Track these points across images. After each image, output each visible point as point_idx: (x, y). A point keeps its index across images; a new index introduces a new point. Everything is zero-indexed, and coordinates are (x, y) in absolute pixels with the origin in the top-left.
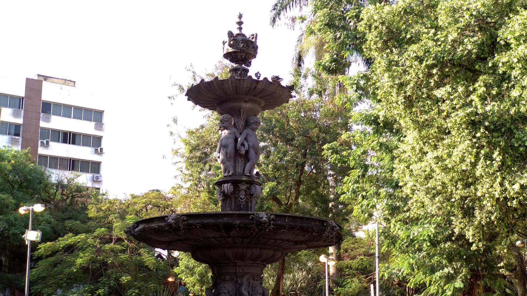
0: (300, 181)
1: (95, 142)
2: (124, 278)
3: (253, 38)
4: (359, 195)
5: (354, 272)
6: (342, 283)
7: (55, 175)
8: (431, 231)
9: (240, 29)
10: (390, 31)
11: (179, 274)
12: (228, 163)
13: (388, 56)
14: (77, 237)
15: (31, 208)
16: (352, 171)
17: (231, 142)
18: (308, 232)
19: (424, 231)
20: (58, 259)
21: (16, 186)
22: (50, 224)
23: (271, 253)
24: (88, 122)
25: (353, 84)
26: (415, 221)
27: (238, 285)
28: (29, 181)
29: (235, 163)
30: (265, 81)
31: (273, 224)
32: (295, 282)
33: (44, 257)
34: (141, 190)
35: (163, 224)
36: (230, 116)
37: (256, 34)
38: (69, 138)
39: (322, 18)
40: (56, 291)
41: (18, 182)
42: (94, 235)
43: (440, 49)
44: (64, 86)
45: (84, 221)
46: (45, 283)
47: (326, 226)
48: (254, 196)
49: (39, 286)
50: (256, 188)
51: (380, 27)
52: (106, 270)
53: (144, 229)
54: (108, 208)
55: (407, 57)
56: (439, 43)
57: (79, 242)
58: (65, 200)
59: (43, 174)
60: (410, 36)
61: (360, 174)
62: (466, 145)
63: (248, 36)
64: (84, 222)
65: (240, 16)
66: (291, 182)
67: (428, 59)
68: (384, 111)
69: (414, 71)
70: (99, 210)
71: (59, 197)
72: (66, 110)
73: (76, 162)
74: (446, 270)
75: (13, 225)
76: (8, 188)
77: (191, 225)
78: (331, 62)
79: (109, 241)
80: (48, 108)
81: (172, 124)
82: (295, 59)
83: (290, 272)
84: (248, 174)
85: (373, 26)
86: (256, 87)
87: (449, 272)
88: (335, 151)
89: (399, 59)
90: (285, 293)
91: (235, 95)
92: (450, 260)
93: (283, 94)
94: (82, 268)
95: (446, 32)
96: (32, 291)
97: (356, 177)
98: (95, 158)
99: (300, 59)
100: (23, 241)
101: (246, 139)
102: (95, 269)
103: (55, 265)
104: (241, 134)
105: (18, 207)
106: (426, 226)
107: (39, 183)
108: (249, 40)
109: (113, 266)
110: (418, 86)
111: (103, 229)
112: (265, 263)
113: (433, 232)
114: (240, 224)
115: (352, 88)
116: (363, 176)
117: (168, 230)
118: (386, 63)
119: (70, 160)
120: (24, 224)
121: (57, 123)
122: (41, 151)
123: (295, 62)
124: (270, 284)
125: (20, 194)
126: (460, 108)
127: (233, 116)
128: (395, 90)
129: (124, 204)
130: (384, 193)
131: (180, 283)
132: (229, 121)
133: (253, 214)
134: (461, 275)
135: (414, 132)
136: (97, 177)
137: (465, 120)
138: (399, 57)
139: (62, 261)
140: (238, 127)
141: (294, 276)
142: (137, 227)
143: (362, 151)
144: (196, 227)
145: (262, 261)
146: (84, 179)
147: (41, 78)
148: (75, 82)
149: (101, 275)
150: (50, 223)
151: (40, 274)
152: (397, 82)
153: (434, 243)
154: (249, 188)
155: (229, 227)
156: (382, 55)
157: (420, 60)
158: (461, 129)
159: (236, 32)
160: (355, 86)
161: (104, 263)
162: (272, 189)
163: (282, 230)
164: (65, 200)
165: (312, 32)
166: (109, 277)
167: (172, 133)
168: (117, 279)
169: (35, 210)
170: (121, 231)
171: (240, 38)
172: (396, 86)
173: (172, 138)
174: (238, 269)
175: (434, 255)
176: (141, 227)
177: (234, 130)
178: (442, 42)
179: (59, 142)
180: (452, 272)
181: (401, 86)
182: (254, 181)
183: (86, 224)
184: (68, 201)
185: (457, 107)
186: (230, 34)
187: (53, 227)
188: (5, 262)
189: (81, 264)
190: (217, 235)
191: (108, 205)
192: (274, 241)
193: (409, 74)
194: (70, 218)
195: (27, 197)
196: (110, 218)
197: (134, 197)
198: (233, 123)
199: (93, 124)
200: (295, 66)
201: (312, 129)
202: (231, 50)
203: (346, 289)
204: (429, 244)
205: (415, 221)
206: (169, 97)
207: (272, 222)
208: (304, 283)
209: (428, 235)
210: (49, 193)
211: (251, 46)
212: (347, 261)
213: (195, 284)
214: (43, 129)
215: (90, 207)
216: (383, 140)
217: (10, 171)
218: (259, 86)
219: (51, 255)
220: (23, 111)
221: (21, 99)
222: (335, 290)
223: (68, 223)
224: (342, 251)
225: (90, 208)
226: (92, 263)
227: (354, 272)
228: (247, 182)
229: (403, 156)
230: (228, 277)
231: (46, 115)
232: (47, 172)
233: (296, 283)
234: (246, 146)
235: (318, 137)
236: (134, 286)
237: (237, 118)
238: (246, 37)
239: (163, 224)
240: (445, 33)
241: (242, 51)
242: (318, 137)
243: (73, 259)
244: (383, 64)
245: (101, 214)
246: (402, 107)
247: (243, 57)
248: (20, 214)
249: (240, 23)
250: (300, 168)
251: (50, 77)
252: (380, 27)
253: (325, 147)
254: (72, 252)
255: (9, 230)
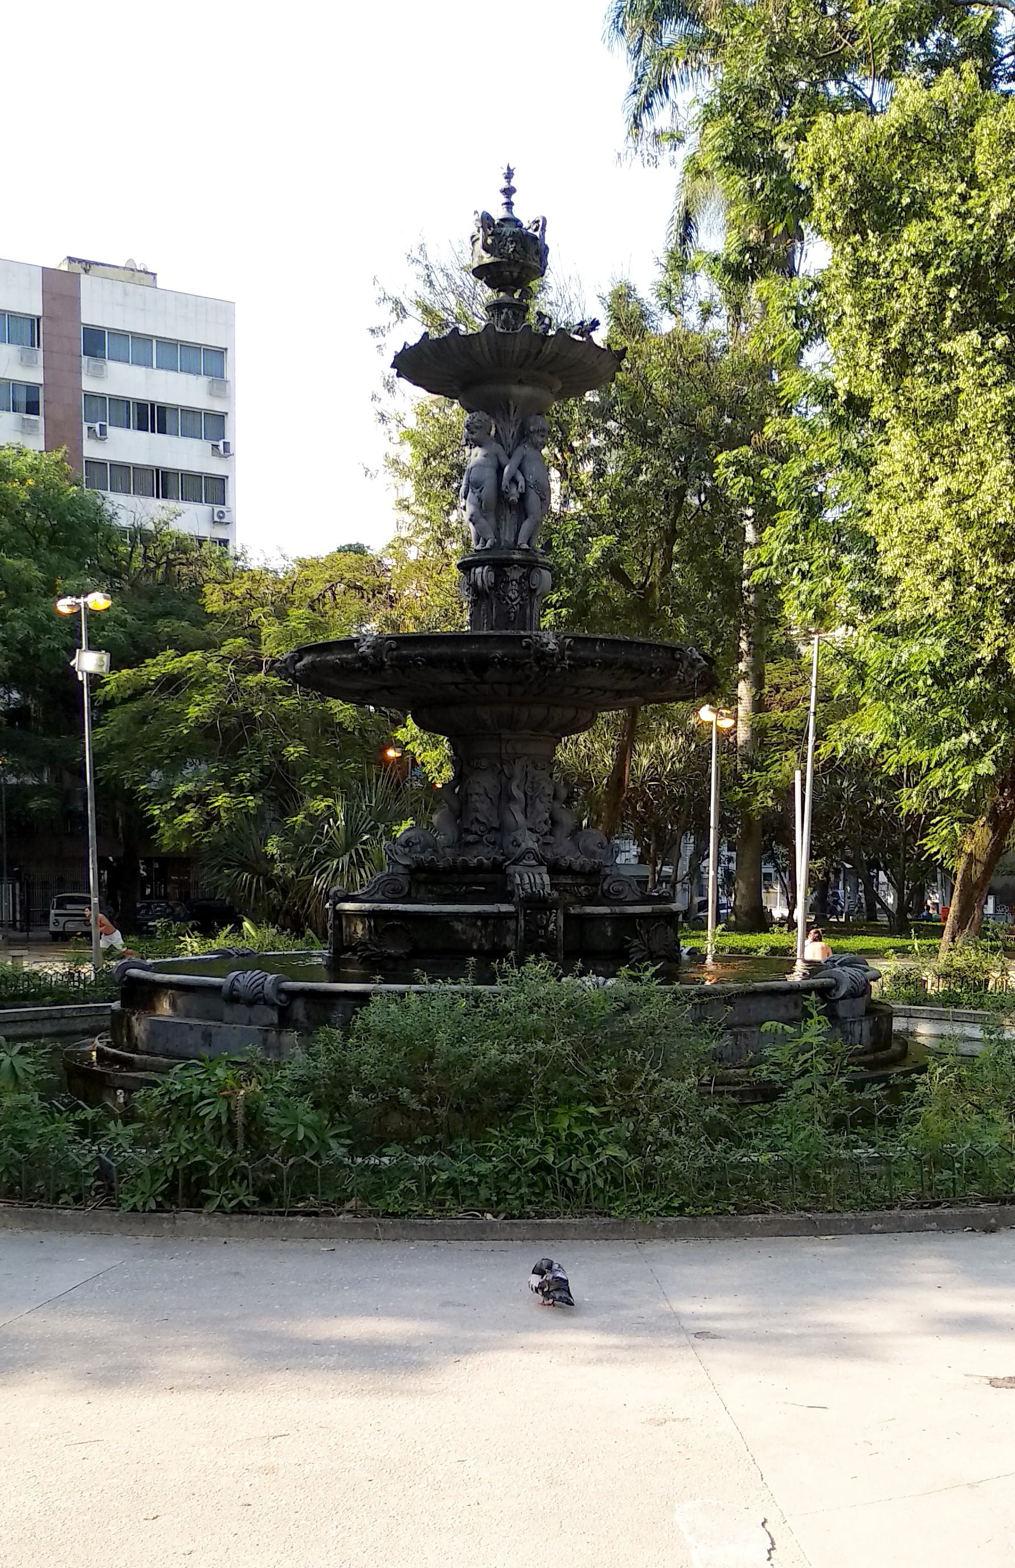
0: (674, 531)
1: (212, 426)
2: (292, 750)
3: (536, 230)
4: (793, 569)
5: (790, 737)
6: (764, 761)
7: (129, 510)
8: (937, 653)
9: (509, 205)
10: (865, 186)
11: (407, 743)
12: (483, 521)
13: (855, 250)
14: (185, 659)
15: (81, 600)
16: (782, 514)
17: (490, 473)
18: (643, 673)
19: (925, 651)
20: (147, 708)
21: (44, 540)
22: (125, 627)
23: (570, 713)
24: (191, 377)
25: (789, 308)
26: (909, 629)
27: (504, 779)
28: (70, 527)
29: (498, 521)
30: (561, 336)
31: (569, 657)
32: (661, 758)
33: (117, 701)
34: (321, 546)
35: (350, 656)
36: (487, 417)
37: (544, 220)
38: (151, 417)
39: (719, 142)
40: (148, 774)
41: (47, 529)
42: (222, 653)
43: (971, 237)
44: (130, 287)
45: (199, 621)
46: (125, 758)
47: (680, 660)
48: (538, 593)
49: (114, 765)
50: (540, 573)
51: (842, 176)
52: (251, 731)
53: (312, 665)
54: (249, 592)
55: (895, 256)
56: (970, 221)
57: (190, 669)
58: (153, 572)
59: (99, 510)
60: (908, 200)
61: (798, 521)
62: (1004, 470)
63: (526, 225)
64: (196, 623)
65: (509, 175)
66: (652, 533)
67: (939, 264)
68: (846, 380)
69: (909, 289)
70: (229, 596)
71: (138, 564)
72: (141, 348)
73: (171, 479)
74: (965, 737)
75: (46, 630)
76: (25, 543)
77: (407, 658)
78: (741, 253)
79: (255, 667)
80: (96, 342)
81: (383, 393)
82: (675, 222)
83: (648, 740)
84: (525, 546)
85: (827, 174)
86: (540, 351)
87: (970, 742)
88: (743, 468)
89: (881, 259)
90: (637, 785)
91: (497, 362)
92: (975, 716)
93: (600, 364)
94: (200, 727)
95: (987, 194)
96: (100, 775)
97: (790, 527)
98: (215, 467)
99: (687, 222)
100: (72, 672)
101: (520, 468)
102: (228, 729)
103: (143, 721)
104: (510, 456)
105: (52, 592)
106: (928, 641)
107: (92, 533)
108: (528, 235)
109: (266, 722)
110: (912, 332)
111: (240, 640)
112: (558, 735)
113: (942, 655)
114: (503, 657)
115: (787, 318)
116: (806, 525)
117: (360, 669)
118: (851, 268)
119: (157, 470)
120: (71, 634)
121: (124, 380)
122: (91, 450)
123: (674, 228)
124: (605, 765)
125: (54, 558)
126: (995, 384)
127: (494, 417)
128: (865, 337)
129: (283, 582)
130: (850, 566)
131: (414, 760)
132: (484, 428)
133: (530, 637)
134: (995, 748)
135: (904, 434)
136: (222, 512)
137: (1004, 412)
138: (879, 255)
139: (157, 709)
140: (504, 442)
141: (658, 747)
142: (300, 660)
143: (804, 468)
144: (415, 663)
145: (551, 732)
146: (189, 519)
147: (77, 268)
148: (154, 274)
149: (242, 740)
150: (123, 624)
151: (112, 739)
152: (869, 317)
153: (940, 677)
154: (526, 577)
155: (480, 664)
156: (843, 249)
157: (923, 261)
158: (995, 434)
159: (498, 213)
160: (792, 315)
161: (248, 717)
162: (607, 552)
163: (588, 669)
164: (153, 572)
165: (700, 172)
166: (259, 747)
167: (383, 416)
168: (277, 752)
169: (91, 606)
170: (279, 645)
171: (508, 229)
172: (867, 326)
173: (382, 428)
174: (503, 746)
175: (943, 706)
176: (307, 660)
177: (496, 447)
178: (978, 219)
179: (129, 427)
180: (977, 741)
181: (880, 325)
182: (537, 561)
183: (200, 630)
184: (160, 571)
185: (990, 382)
186: (486, 220)
187: (131, 635)
188: (35, 712)
189: (197, 717)
190: (459, 678)
191: (248, 585)
192: (573, 690)
193: (898, 296)
194: (166, 614)
195: (71, 565)
196: (254, 617)
197: (303, 565)
198: (493, 432)
199: (203, 381)
200: (675, 239)
201: (700, 407)
202: (487, 259)
203: (771, 775)
204: (930, 682)
205: (909, 629)
206: (373, 331)
207: (567, 653)
208: (680, 762)
209: (930, 662)
210: (116, 556)
211: (532, 250)
212: (777, 714)
213: (441, 765)
214: (90, 396)
215: (208, 589)
216: (852, 443)
217: (28, 505)
218: (548, 349)
219: (132, 698)
220: (41, 349)
221: (35, 322)
222: (746, 777)
223: (164, 626)
224: (766, 690)
225: (208, 592)
226: (222, 715)
227: (790, 737)
228: (522, 564)
229: (890, 484)
230: (484, 763)
231: (93, 362)
232: (107, 506)
233: (662, 763)
234: (522, 483)
235: (715, 426)
236: (314, 767)
237: (501, 419)
238: (521, 226)
239: (350, 656)
240: (985, 196)
241: (512, 262)
242: (715, 426)
243: (179, 706)
244: (844, 271)
245: (234, 605)
246: (877, 375)
247: (515, 274)
248: (59, 613)
249: (508, 192)
250: (674, 500)
251: (97, 264)
252: (842, 176)
253: (721, 458)
254: (177, 691)
255: (37, 641)
